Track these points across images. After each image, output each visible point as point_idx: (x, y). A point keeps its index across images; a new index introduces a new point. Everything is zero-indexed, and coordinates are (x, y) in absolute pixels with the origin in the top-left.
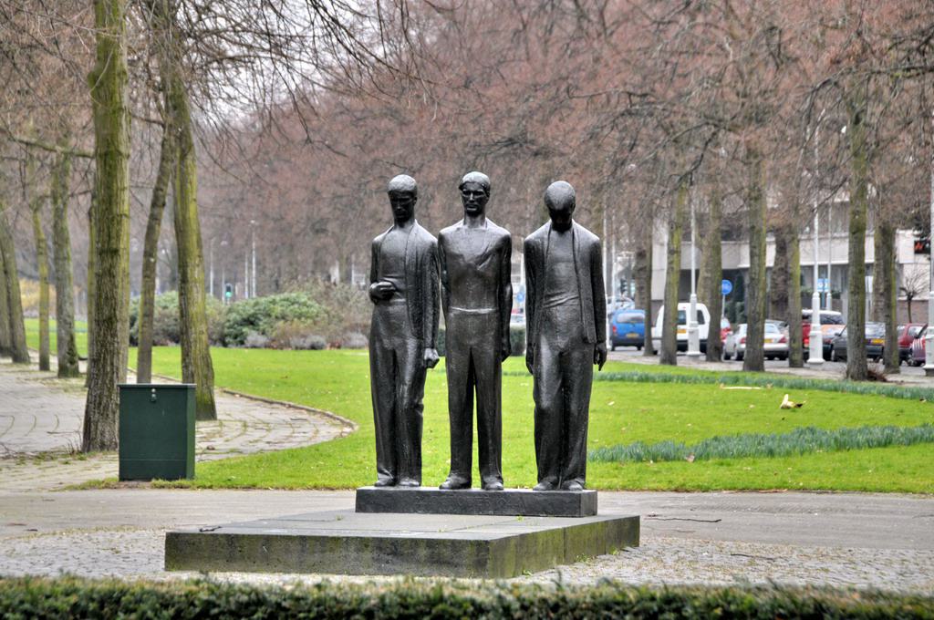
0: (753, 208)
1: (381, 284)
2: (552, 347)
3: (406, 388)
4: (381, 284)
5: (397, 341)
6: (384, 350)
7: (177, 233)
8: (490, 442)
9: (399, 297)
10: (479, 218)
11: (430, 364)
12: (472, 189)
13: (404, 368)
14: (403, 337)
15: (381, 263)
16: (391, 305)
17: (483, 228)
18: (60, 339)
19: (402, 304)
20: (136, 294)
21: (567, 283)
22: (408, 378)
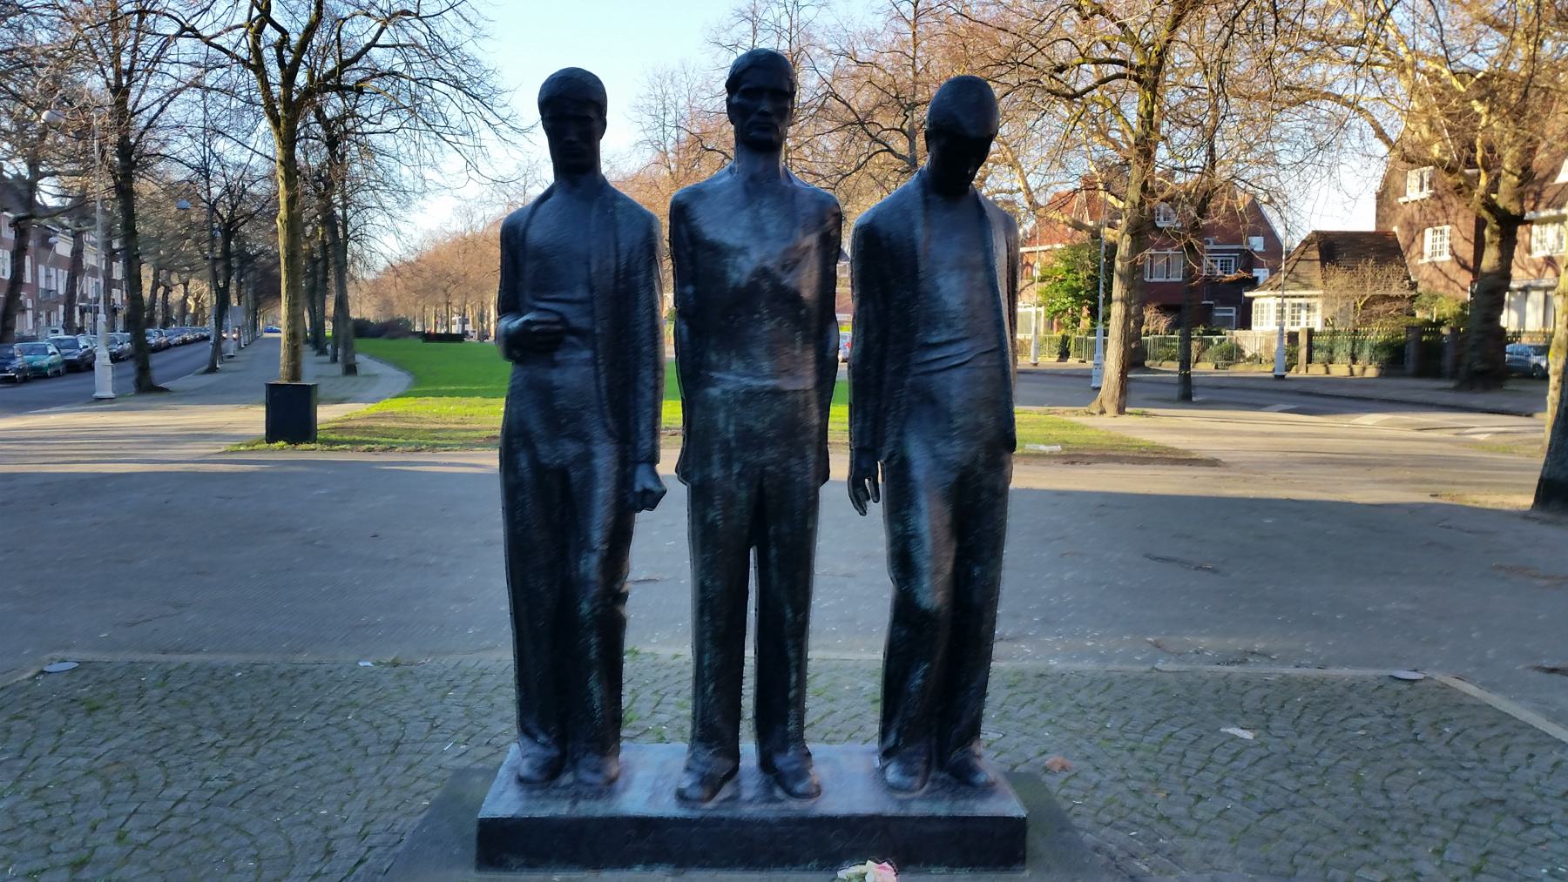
3: (594, 560)
5: (571, 449)
6: (537, 466)
7: (1126, 316)
9: (574, 346)
11: (649, 499)
13: (587, 512)
14: (582, 437)
15: (530, 267)
16: (555, 365)
18: (372, 427)
21: (1116, 300)
22: (598, 536)
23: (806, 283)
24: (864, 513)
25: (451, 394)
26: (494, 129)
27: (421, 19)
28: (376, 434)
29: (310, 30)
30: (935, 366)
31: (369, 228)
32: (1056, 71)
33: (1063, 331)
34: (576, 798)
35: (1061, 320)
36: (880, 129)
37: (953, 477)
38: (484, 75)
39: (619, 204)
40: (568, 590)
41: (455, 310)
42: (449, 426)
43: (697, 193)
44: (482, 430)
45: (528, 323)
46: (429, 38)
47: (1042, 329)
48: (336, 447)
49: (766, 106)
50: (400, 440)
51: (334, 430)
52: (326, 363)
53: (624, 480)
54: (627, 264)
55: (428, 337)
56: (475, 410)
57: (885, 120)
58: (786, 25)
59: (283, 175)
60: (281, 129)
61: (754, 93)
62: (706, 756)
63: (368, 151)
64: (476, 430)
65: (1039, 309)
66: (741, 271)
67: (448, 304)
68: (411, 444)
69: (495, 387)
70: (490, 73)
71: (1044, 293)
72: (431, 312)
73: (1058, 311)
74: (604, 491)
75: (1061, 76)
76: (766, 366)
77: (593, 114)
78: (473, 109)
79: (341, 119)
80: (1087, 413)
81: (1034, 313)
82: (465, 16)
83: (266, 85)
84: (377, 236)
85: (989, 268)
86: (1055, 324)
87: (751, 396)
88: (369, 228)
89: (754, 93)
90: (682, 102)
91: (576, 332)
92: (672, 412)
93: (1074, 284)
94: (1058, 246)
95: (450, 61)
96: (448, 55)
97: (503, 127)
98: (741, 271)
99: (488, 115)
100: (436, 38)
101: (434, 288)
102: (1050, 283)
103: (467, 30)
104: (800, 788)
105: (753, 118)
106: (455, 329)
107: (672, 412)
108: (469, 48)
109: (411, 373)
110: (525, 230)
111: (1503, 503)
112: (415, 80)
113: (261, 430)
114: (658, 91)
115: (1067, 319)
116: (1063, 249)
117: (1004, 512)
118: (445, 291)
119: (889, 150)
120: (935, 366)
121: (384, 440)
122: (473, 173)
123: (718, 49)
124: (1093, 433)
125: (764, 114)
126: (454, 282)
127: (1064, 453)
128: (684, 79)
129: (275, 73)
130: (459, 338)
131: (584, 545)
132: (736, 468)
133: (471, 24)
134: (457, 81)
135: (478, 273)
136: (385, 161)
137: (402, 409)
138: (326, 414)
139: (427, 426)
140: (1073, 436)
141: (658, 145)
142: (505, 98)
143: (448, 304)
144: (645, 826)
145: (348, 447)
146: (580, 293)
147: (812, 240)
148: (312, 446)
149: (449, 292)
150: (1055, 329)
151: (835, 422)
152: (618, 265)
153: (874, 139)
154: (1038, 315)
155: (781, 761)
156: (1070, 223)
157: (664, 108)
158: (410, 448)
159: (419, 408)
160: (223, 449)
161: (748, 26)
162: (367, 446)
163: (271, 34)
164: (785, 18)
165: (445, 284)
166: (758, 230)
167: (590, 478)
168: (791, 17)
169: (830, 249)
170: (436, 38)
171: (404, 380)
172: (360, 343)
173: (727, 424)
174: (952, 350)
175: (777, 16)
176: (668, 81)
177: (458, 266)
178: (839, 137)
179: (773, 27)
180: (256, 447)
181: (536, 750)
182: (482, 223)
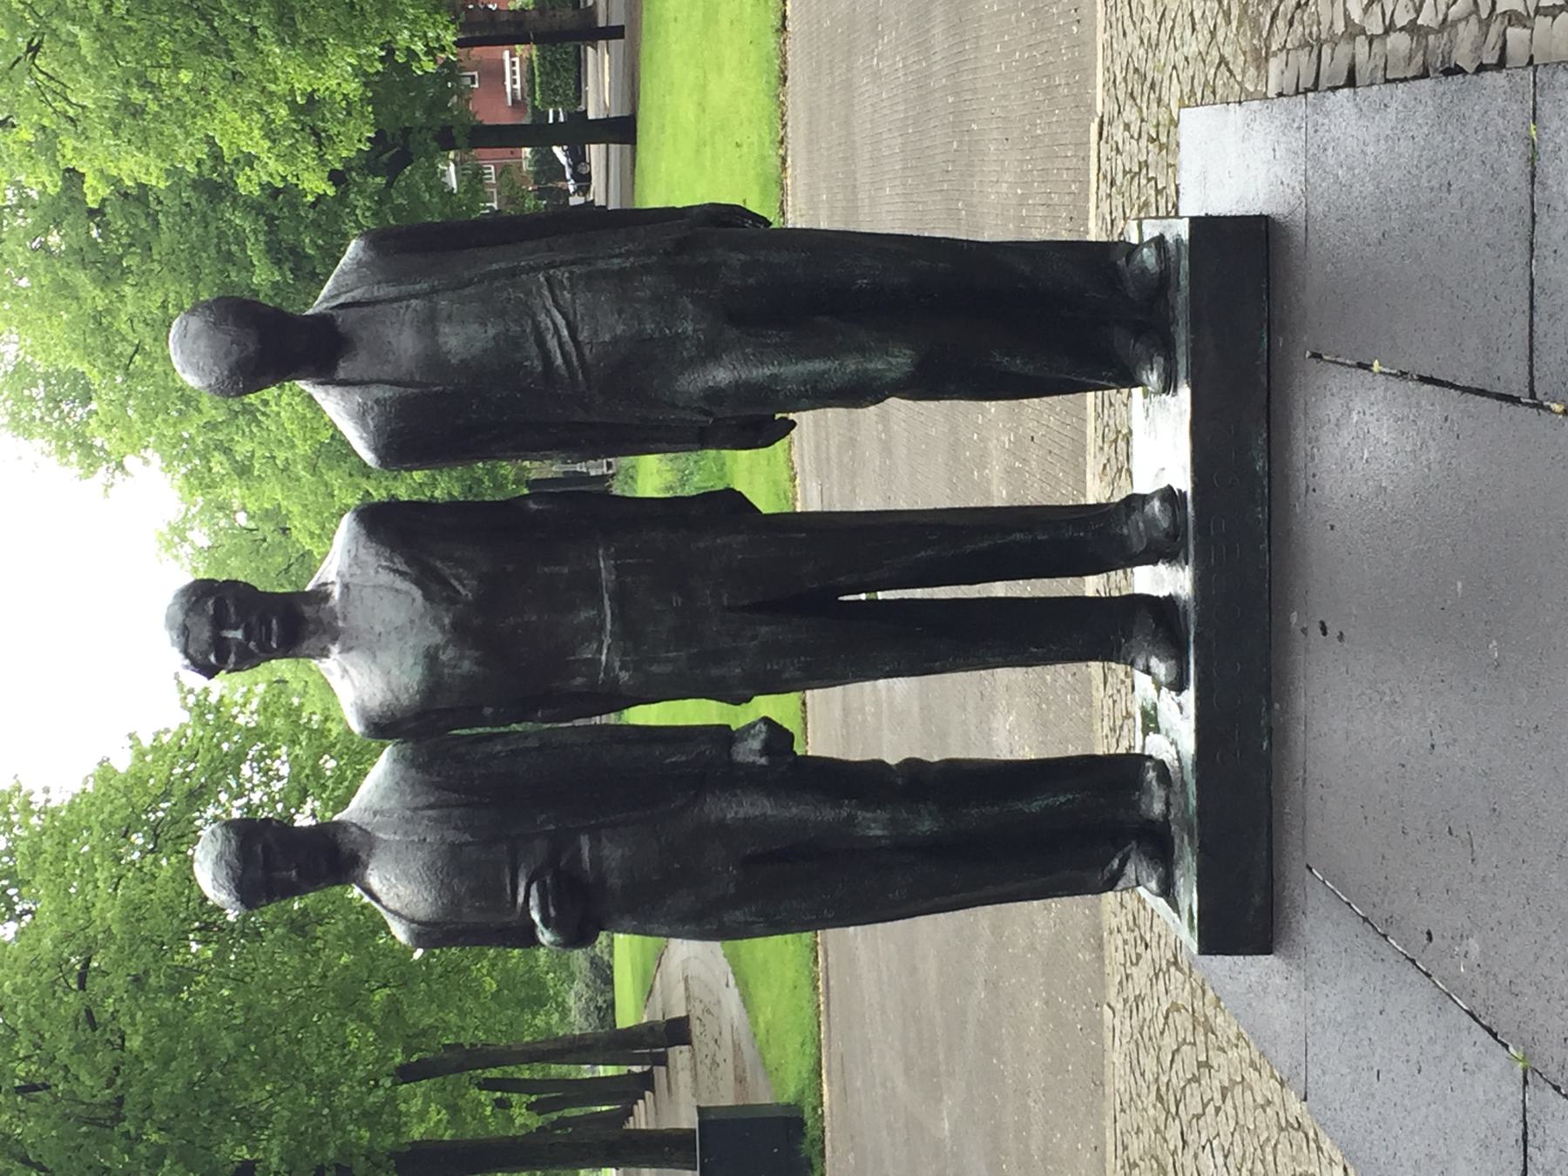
0: (123, 448)
1: (535, 916)
2: (711, 352)
4: (535, 916)
8: (1018, 536)
10: (308, 611)
12: (206, 634)
17: (336, 592)
19: (596, 842)
20: (536, 997)
53: (749, 779)
54: (456, 792)
110: (420, 923)
111: (550, 249)
117: (971, 761)
151: (647, 1123)
152: (458, 806)
173: (668, 660)
174: (553, 344)
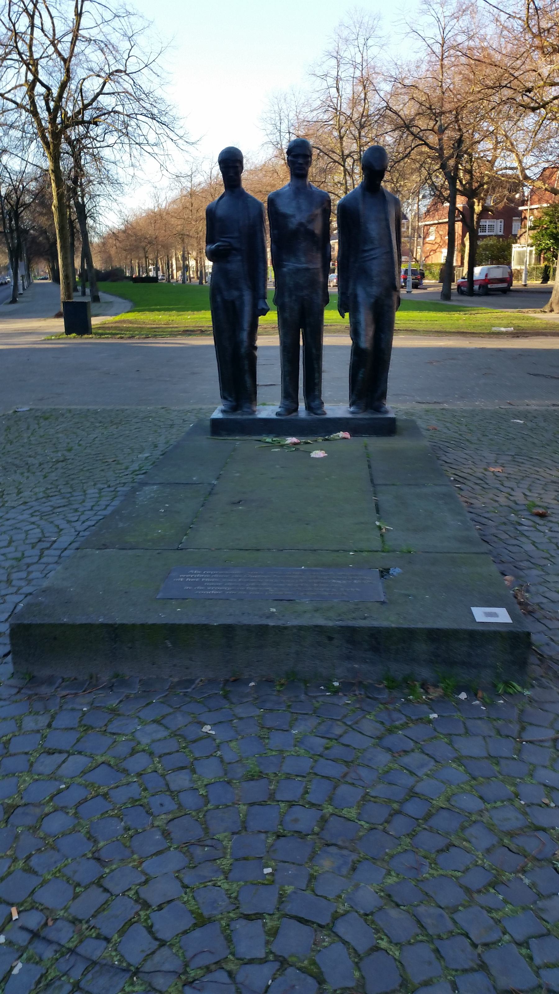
5: (236, 293)
14: (239, 289)
23: (317, 228)
24: (343, 317)
25: (159, 310)
26: (175, 143)
27: (128, 75)
28: (122, 330)
29: (63, 86)
30: (367, 259)
31: (98, 208)
32: (526, 91)
33: (546, 263)
34: (242, 415)
35: (546, 255)
36: (419, 130)
37: (372, 300)
38: (168, 109)
39: (249, 199)
40: (237, 344)
41: (150, 261)
42: (161, 326)
43: (277, 194)
44: (180, 327)
45: (218, 246)
46: (134, 87)
47: (533, 261)
48: (103, 336)
49: (301, 161)
50: (136, 333)
51: (99, 328)
52: (79, 296)
53: (255, 305)
55: (139, 280)
56: (174, 318)
57: (422, 123)
58: (359, 60)
59: (54, 178)
60: (51, 150)
61: (296, 156)
62: (287, 403)
63: (96, 158)
64: (176, 327)
65: (532, 248)
66: (293, 223)
67: (146, 258)
68: (143, 335)
69: (183, 306)
70: (171, 107)
71: (535, 238)
72: (135, 263)
73: (543, 249)
74: (247, 309)
75: (532, 94)
76: (303, 259)
77: (238, 165)
78: (162, 131)
79: (78, 141)
80: (541, 311)
81: (528, 251)
82: (154, 71)
83: (39, 121)
84: (103, 214)
85: (387, 220)
86: (542, 258)
87: (298, 270)
88: (98, 208)
89: (296, 156)
90: (292, 115)
91: (235, 249)
92: (271, 274)
93: (554, 231)
94: (545, 205)
95: (148, 101)
96: (146, 98)
97: (180, 142)
98: (293, 223)
99: (172, 135)
100: (138, 87)
101: (137, 247)
102: (539, 230)
103: (156, 80)
104: (319, 412)
105: (297, 165)
106: (152, 274)
107: (271, 274)
108: (158, 93)
109: (131, 301)
112: (127, 116)
113: (63, 330)
114: (276, 108)
115: (549, 255)
116: (548, 207)
118: (144, 249)
119: (426, 144)
120: (367, 259)
121: (128, 333)
122: (165, 172)
123: (314, 78)
124: (539, 321)
125: (301, 164)
126: (149, 243)
127: (515, 331)
128: (293, 99)
129: (44, 115)
130: (155, 280)
131: (242, 329)
132: (294, 298)
133: (158, 76)
134: (152, 114)
135: (165, 236)
136: (110, 166)
137: (133, 318)
138: (95, 321)
139: (148, 326)
140: (523, 324)
141: (276, 145)
142: (181, 123)
143: (146, 258)
144: (266, 421)
145: (110, 336)
146: (236, 234)
147: (318, 211)
148: (90, 336)
149: (146, 249)
150: (542, 262)
153: (415, 136)
154: (531, 252)
155: (313, 405)
156: (549, 189)
157: (280, 119)
158: (143, 336)
159: (142, 317)
160: (43, 339)
161: (334, 62)
162: (120, 336)
163: (39, 89)
164: (359, 56)
165: (143, 244)
166: (299, 208)
167: (242, 304)
168: (362, 54)
169: (327, 213)
170: (138, 87)
171: (129, 305)
172: (100, 285)
174: (372, 252)
175: (353, 54)
176: (283, 101)
177: (151, 232)
178: (396, 134)
179: (351, 62)
180: (61, 337)
181: (228, 403)
182: (165, 202)
